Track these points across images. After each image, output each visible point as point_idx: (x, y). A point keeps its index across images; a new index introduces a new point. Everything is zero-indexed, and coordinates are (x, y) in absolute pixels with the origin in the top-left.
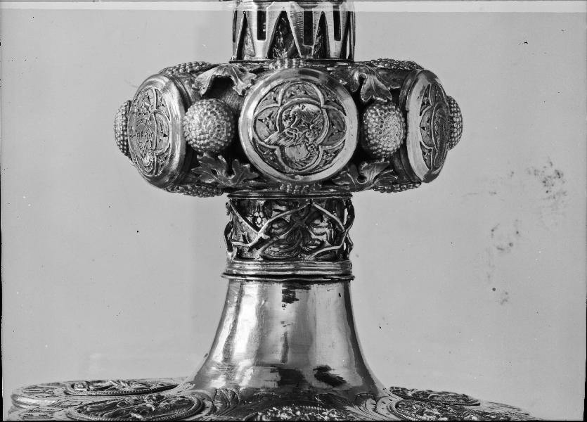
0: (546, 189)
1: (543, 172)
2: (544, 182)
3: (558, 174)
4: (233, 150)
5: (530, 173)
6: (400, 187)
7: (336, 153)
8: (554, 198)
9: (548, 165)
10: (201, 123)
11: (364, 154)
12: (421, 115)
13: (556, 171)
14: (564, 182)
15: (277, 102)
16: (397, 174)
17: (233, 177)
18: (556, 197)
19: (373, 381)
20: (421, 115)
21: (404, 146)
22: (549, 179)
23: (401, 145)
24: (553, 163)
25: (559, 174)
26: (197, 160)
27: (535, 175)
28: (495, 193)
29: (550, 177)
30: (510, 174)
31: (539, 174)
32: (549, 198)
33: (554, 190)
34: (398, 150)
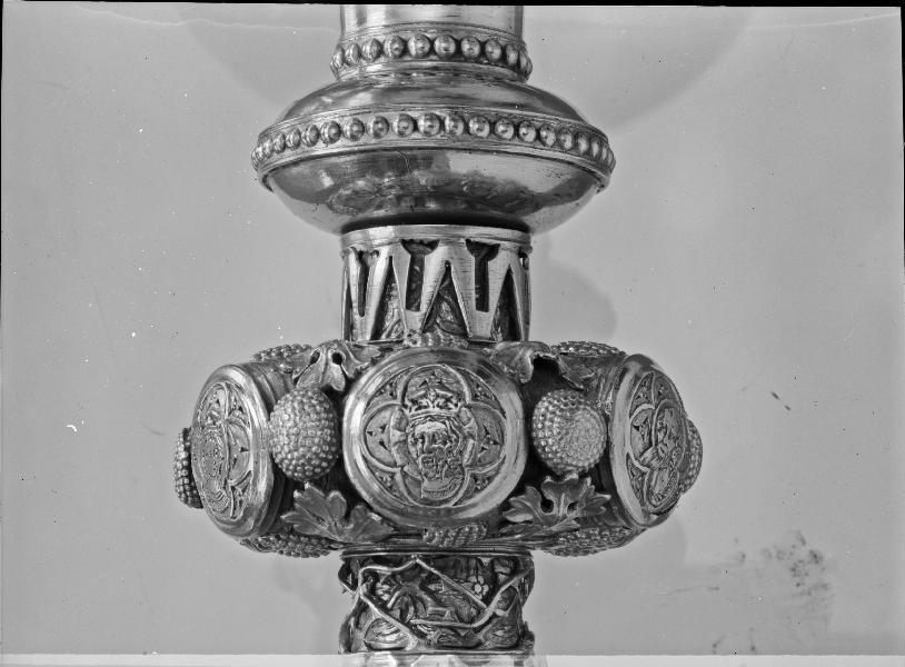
0: (798, 580)
1: (791, 554)
2: (793, 570)
3: (815, 556)
4: (333, 475)
5: (770, 556)
6: (600, 533)
7: (490, 479)
8: (809, 593)
9: (798, 543)
10: (290, 430)
11: (537, 470)
12: (631, 415)
13: (811, 552)
14: (823, 569)
15: (395, 398)
16: (603, 515)
17: (352, 526)
18: (813, 592)
19: (574, 111)
20: (631, 415)
21: (605, 461)
22: (801, 565)
23: (601, 458)
24: (807, 540)
25: (815, 557)
26: (293, 500)
27: (779, 558)
28: (717, 589)
29: (800, 561)
30: (741, 558)
31: (785, 557)
32: (802, 594)
33: (809, 581)
34: (597, 465)
